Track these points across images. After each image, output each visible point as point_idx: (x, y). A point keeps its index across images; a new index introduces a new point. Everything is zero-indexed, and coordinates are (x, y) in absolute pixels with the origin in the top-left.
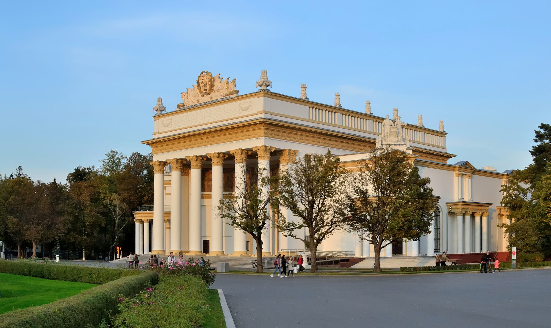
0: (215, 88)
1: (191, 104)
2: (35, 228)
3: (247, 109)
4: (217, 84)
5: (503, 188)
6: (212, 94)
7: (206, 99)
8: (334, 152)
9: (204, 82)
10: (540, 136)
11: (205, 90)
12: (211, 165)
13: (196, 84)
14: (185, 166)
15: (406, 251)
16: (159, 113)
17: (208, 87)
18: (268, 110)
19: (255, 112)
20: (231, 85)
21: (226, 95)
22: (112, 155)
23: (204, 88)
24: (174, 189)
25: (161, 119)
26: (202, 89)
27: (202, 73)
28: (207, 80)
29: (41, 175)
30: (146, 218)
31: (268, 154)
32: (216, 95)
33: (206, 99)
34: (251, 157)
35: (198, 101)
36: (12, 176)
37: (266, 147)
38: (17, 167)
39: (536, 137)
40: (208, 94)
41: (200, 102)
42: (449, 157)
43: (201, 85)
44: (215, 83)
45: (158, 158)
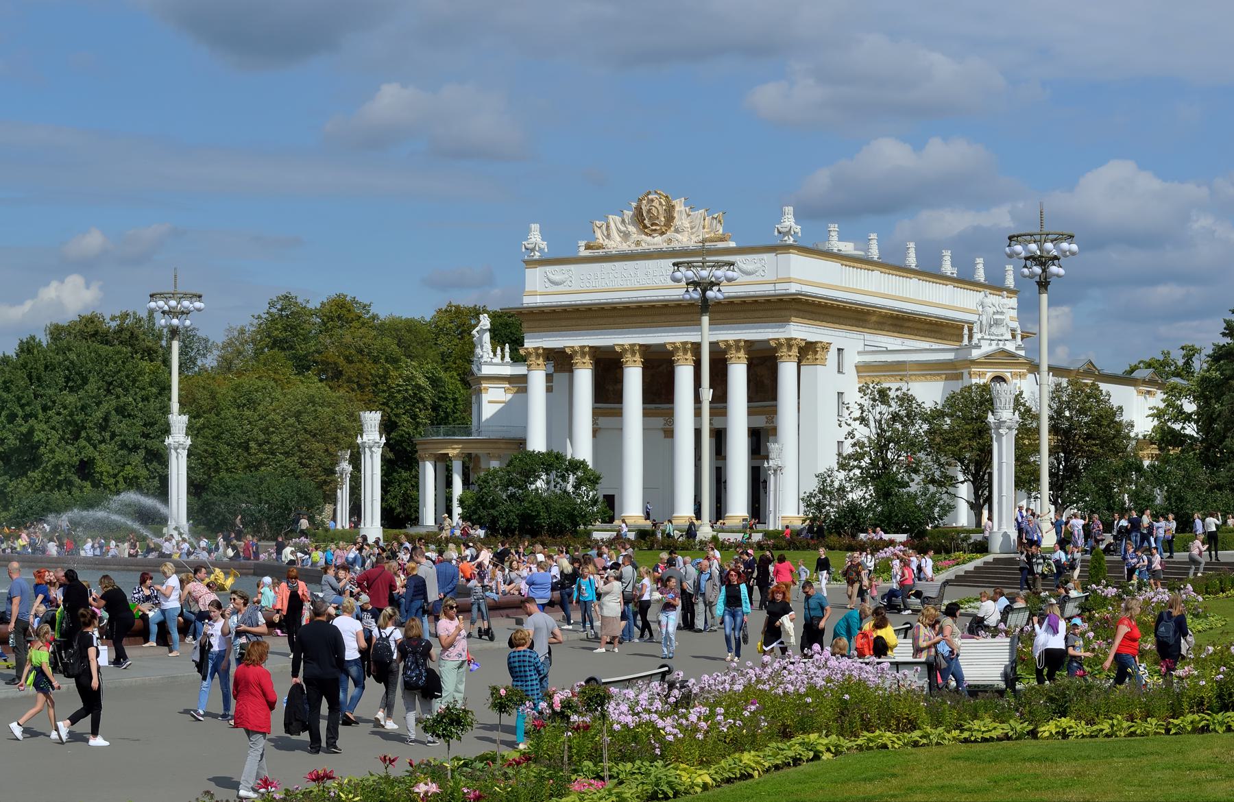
33: (658, 242)
40: (662, 233)
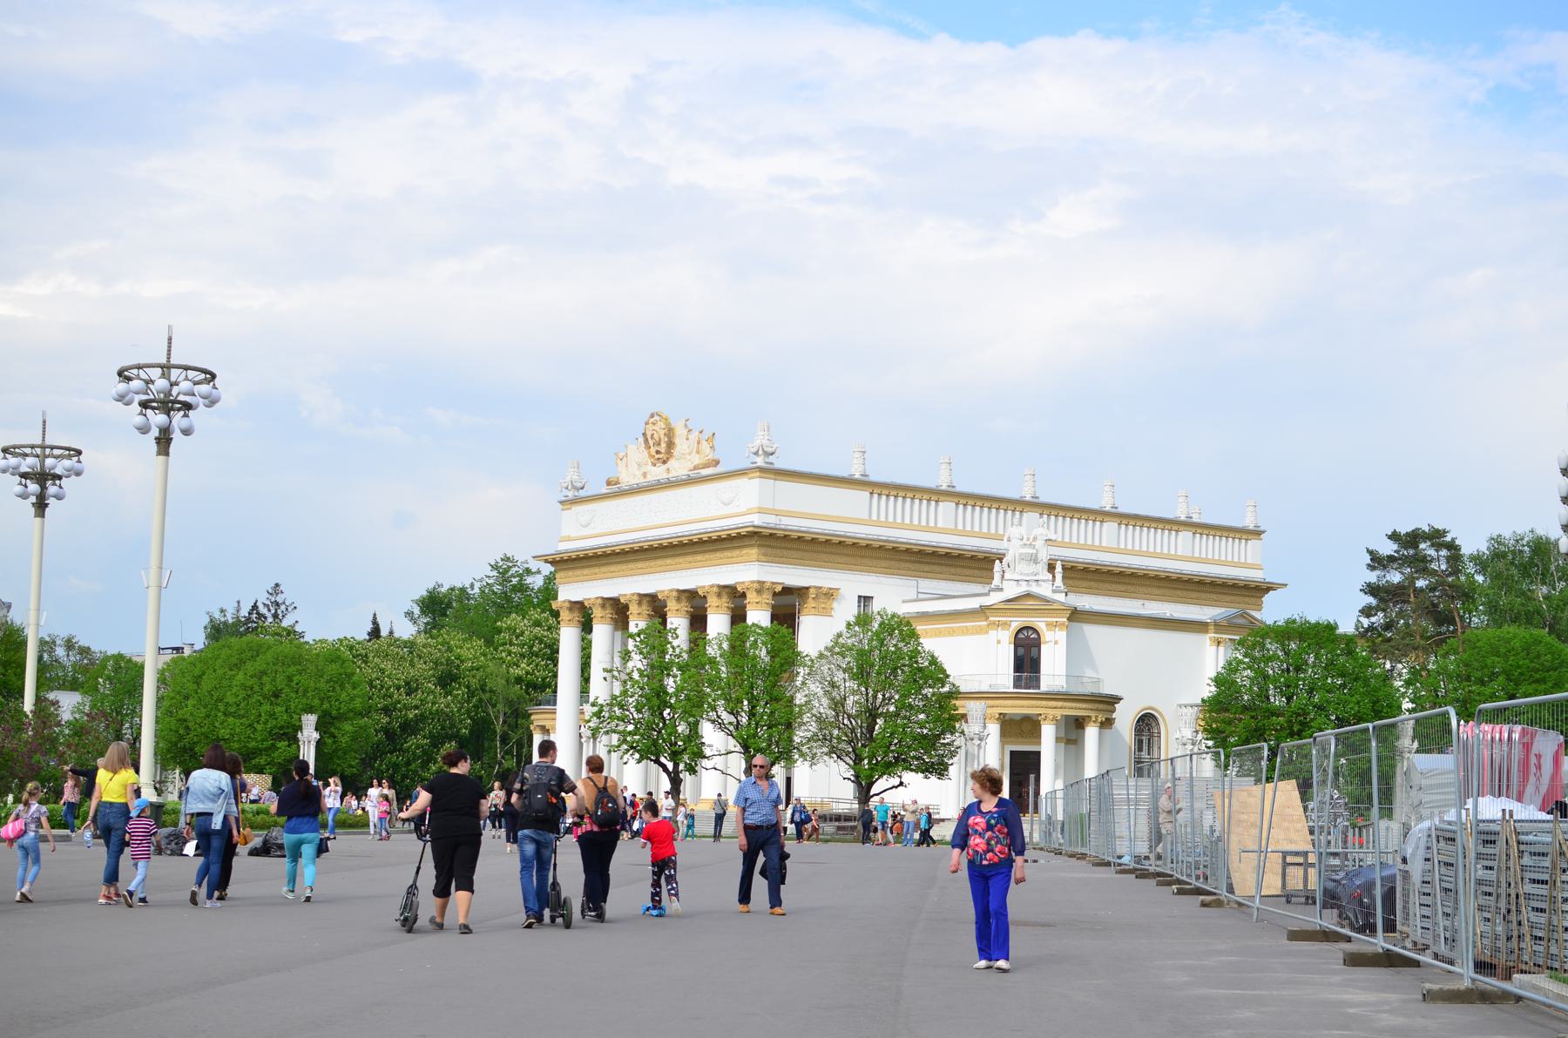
0: (677, 451)
2: (539, 572)
6: (672, 463)
7: (658, 473)
10: (1377, 561)
16: (571, 494)
18: (769, 505)
19: (743, 509)
20: (705, 446)
21: (695, 468)
25: (576, 509)
26: (653, 450)
27: (652, 416)
28: (662, 433)
29: (326, 620)
31: (767, 598)
32: (679, 467)
34: (736, 599)
35: (645, 475)
36: (255, 607)
37: (761, 583)
38: (270, 586)
41: (649, 478)
42: (1268, 590)
44: (677, 441)
45: (569, 592)
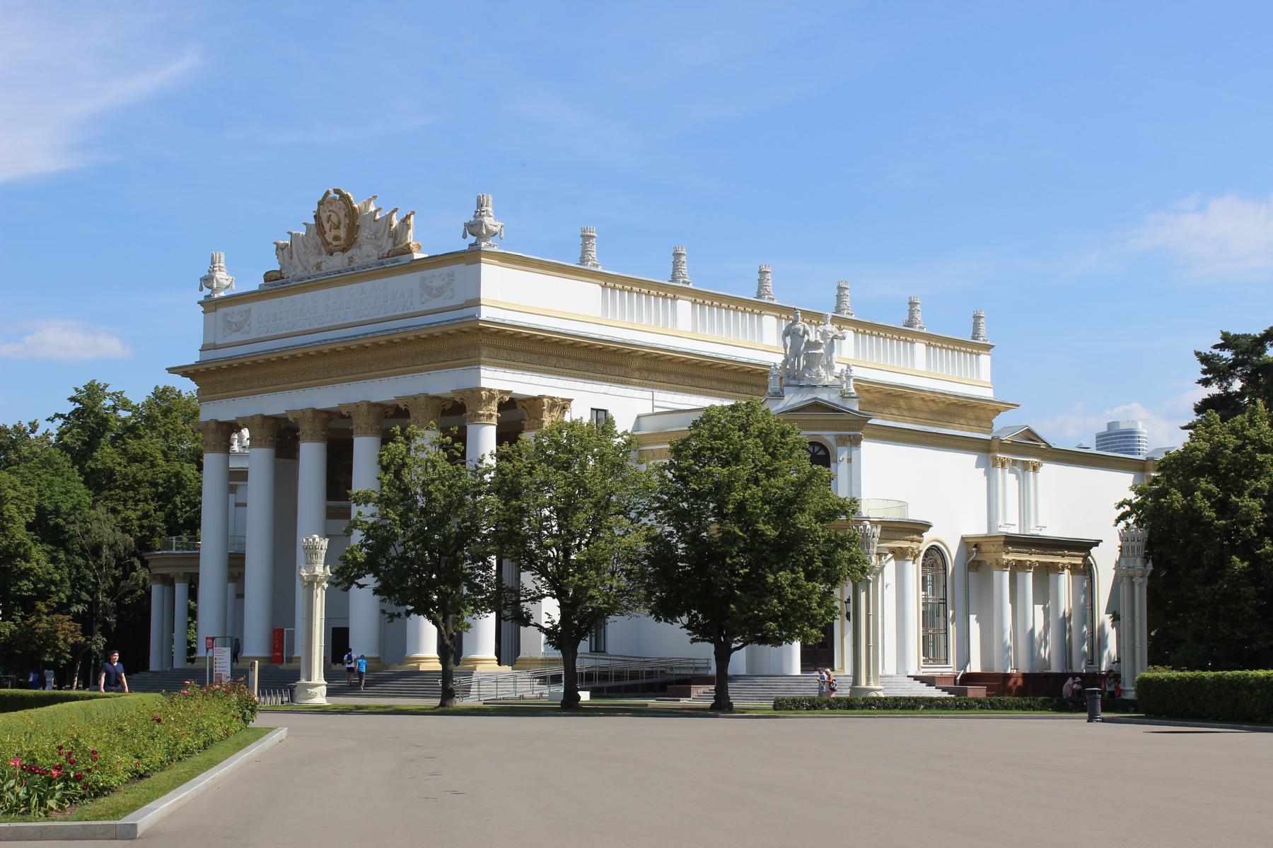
1: (299, 272)
3: (440, 291)
4: (364, 234)
5: (1122, 510)
8: (834, 444)
9: (334, 219)
11: (336, 238)
12: (351, 432)
13: (313, 222)
14: (282, 437)
15: (868, 680)
17: (342, 233)
22: (157, 387)
23: (334, 233)
24: (258, 491)
28: (342, 214)
30: (181, 571)
33: (338, 261)
39: (1204, 372)
40: (344, 250)
43: (327, 226)
